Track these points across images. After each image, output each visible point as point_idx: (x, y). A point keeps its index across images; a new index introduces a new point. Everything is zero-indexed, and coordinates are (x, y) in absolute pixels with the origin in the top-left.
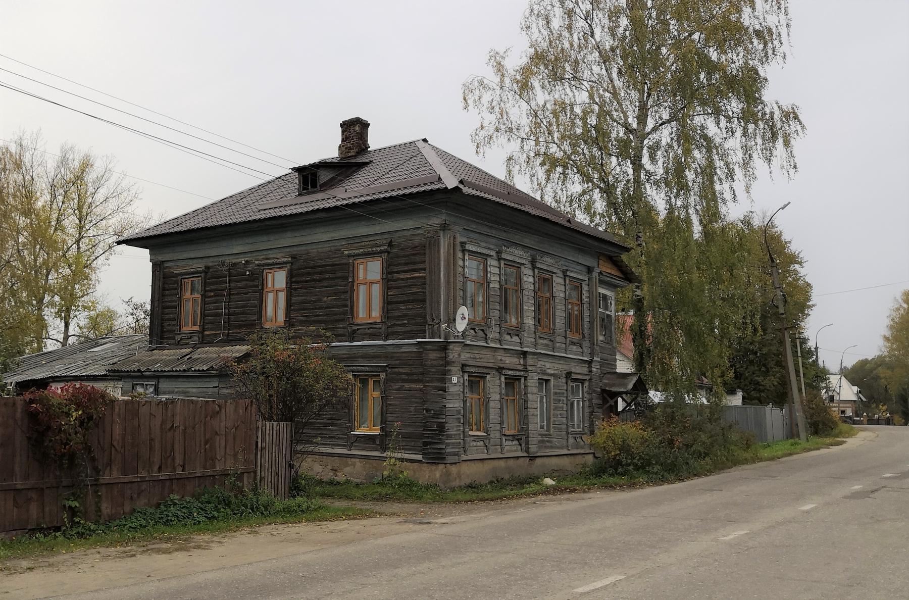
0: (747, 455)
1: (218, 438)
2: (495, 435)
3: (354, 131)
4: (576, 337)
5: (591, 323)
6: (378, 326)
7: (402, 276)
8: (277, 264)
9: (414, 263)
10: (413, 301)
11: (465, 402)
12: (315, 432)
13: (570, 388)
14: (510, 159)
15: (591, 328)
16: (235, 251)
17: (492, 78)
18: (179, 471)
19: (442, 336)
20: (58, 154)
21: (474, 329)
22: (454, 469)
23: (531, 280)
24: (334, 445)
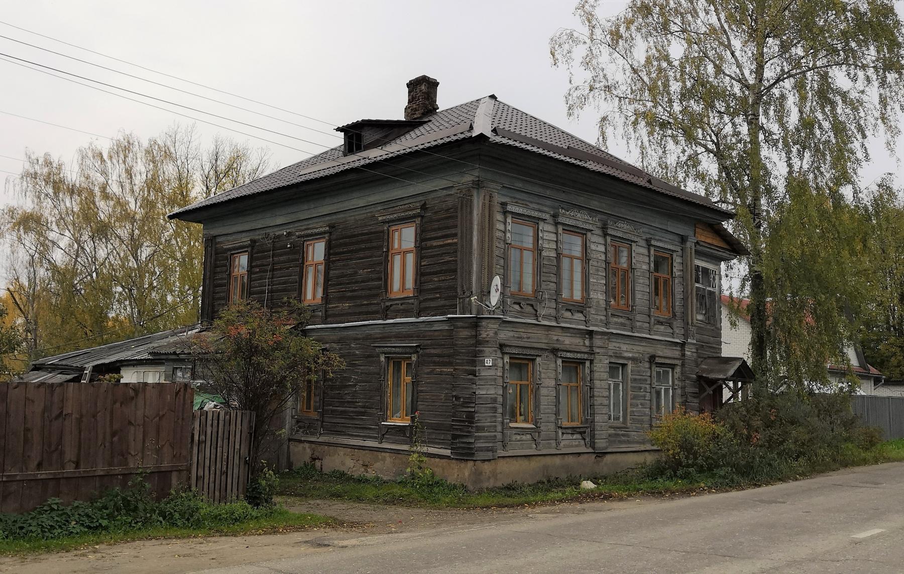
0: (868, 455)
1: (132, 428)
2: (547, 428)
3: (423, 90)
4: (664, 315)
5: (685, 299)
6: (410, 301)
7: (435, 243)
8: (316, 234)
9: (448, 228)
10: (446, 271)
11: (505, 388)
12: (347, 421)
13: (654, 374)
14: (604, 119)
15: (685, 306)
16: (276, 222)
17: (582, 31)
18: (70, 469)
19: (474, 310)
20: (212, 147)
21: (519, 304)
22: (487, 467)
23: (602, 248)
24: (365, 437)
